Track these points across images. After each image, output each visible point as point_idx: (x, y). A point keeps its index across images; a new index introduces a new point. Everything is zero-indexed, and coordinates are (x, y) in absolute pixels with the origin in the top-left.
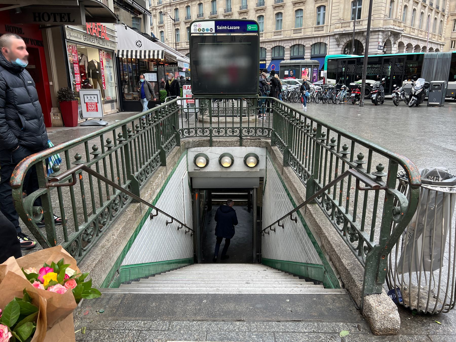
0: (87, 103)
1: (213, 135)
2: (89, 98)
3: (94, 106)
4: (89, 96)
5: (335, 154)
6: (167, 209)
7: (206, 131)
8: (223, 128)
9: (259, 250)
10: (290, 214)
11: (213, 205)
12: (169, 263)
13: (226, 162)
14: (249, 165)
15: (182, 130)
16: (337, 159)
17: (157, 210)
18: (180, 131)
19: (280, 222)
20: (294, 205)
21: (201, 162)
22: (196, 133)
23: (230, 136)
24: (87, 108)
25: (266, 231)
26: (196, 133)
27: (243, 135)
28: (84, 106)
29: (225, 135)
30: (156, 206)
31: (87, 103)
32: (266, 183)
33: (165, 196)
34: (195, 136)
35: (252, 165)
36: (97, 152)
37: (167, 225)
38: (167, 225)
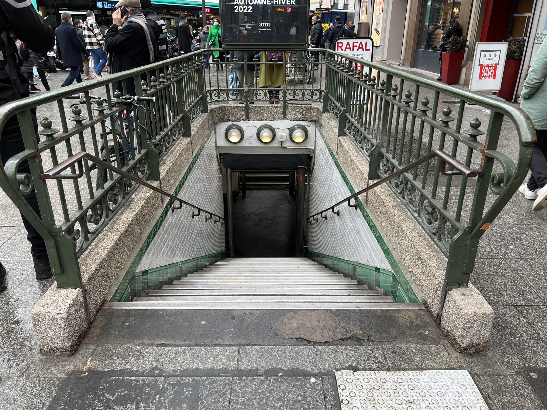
0: (482, 66)
1: (287, 99)
2: (488, 57)
3: (491, 69)
4: (488, 54)
5: (429, 122)
6: (192, 200)
7: (316, 94)
8: (300, 90)
9: (305, 239)
10: (348, 199)
11: (176, 195)
12: (212, 256)
13: (266, 136)
14: (263, 140)
15: (211, 92)
16: (433, 128)
17: (181, 201)
18: (208, 94)
19: (335, 208)
20: (351, 190)
21: (234, 137)
22: (303, 95)
23: (216, 101)
24: (481, 72)
25: (315, 217)
26: (303, 95)
27: (287, 99)
28: (476, 70)
29: (302, 99)
30: (178, 197)
31: (482, 66)
32: (314, 164)
33: (189, 185)
34: (318, 100)
35: (266, 140)
36: (472, 132)
37: (193, 217)
38: (193, 217)
